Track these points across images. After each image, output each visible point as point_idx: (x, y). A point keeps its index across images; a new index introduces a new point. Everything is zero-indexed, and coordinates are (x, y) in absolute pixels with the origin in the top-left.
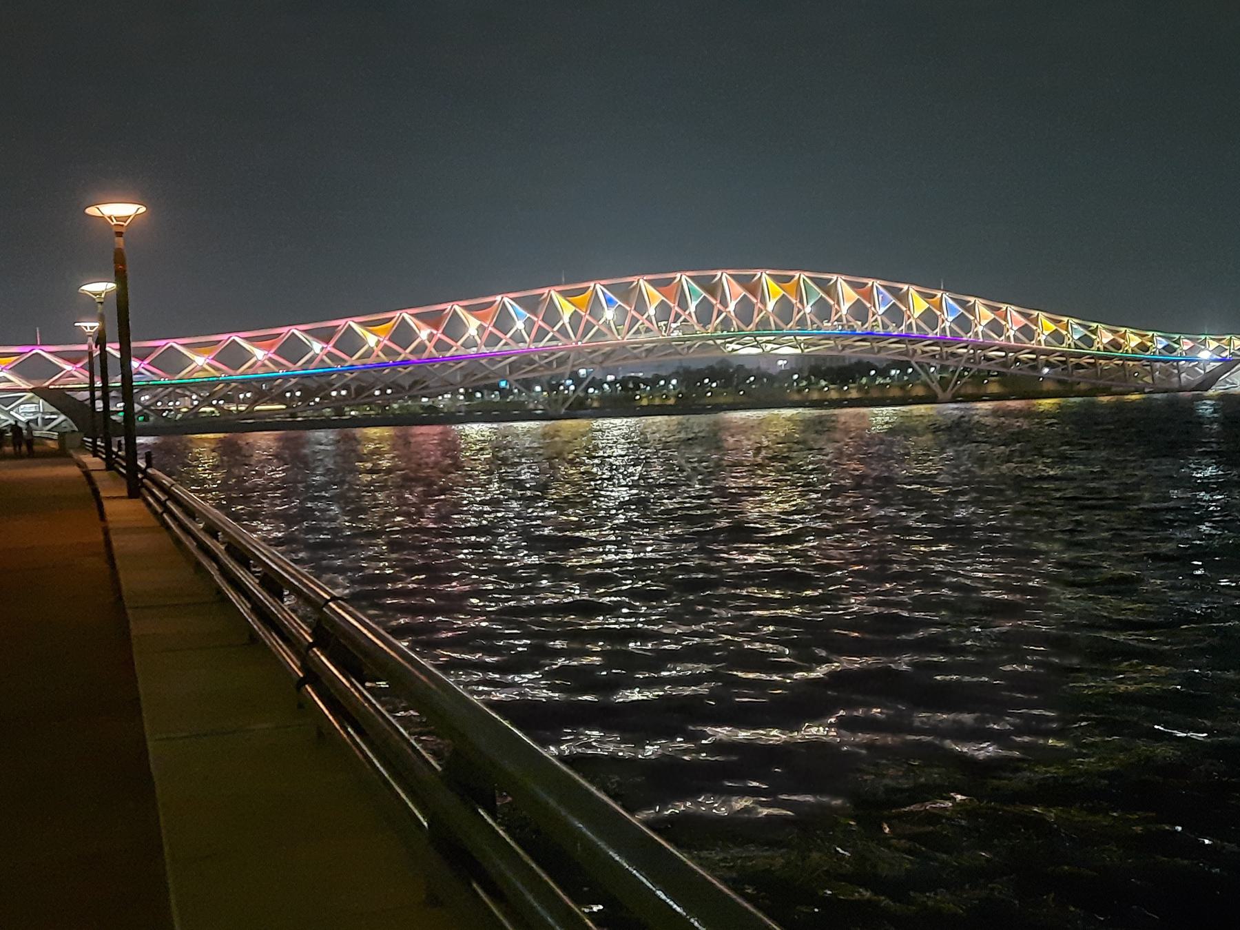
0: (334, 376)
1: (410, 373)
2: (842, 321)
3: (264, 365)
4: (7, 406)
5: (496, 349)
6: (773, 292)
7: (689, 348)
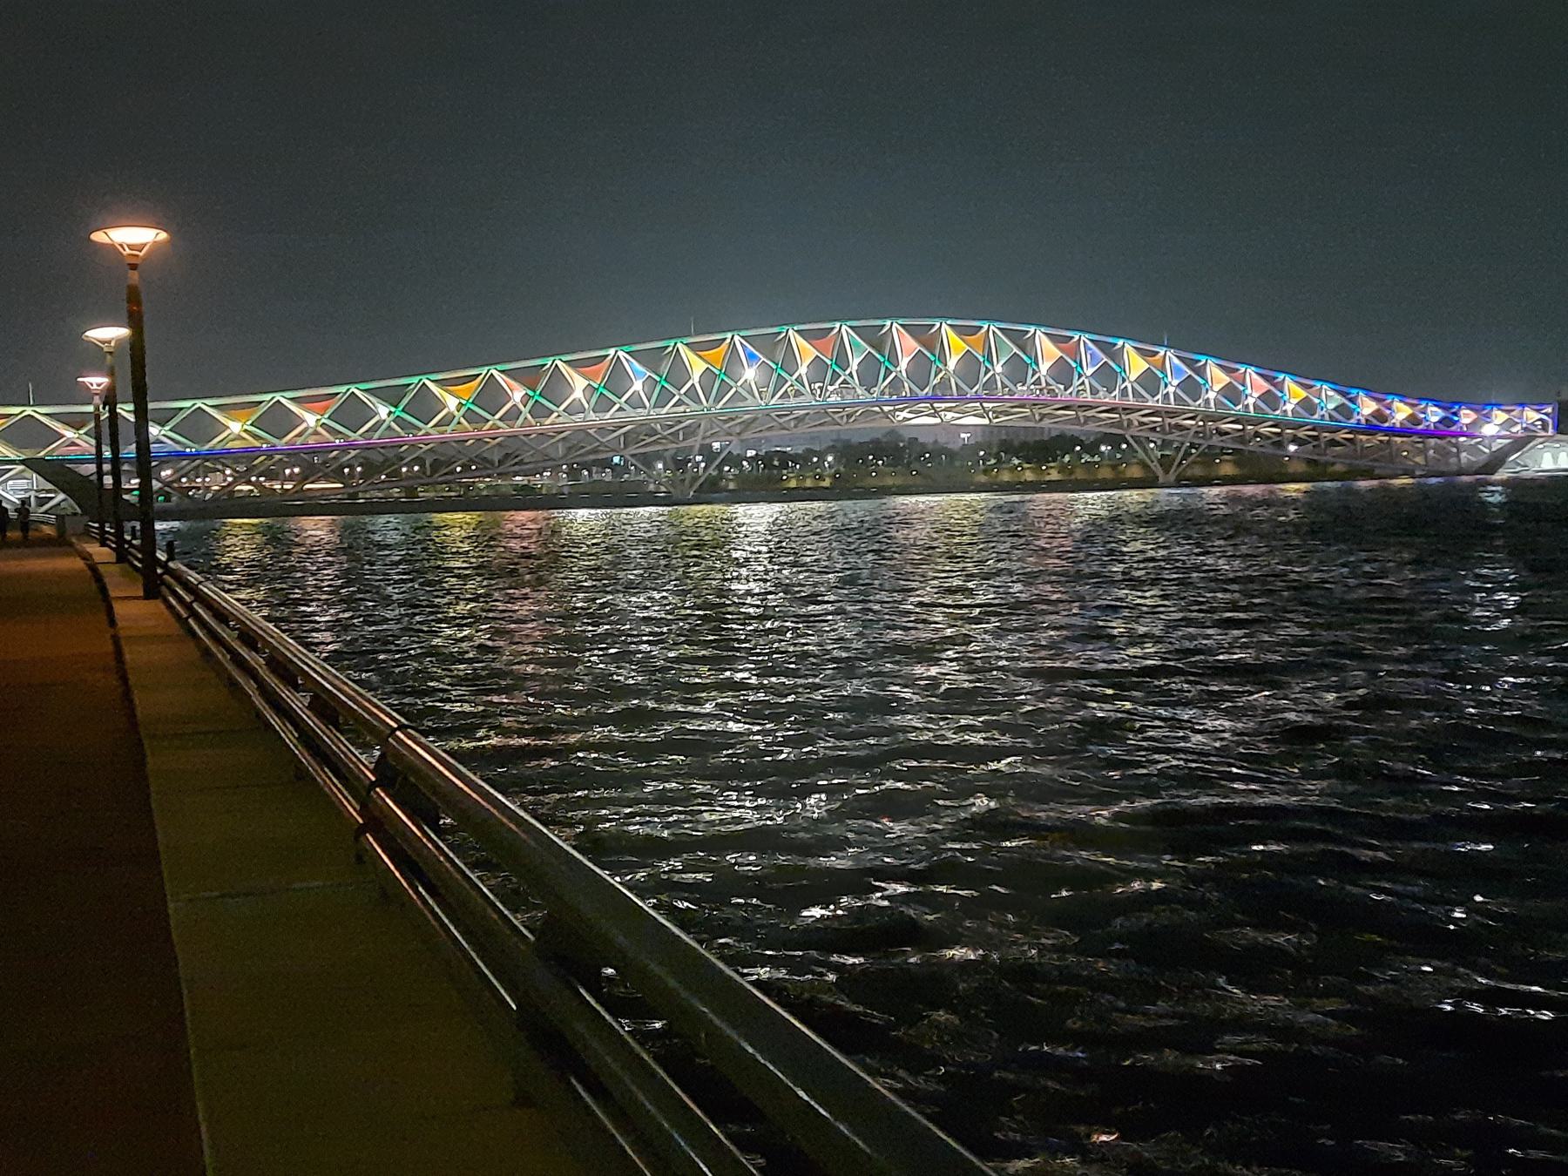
0: (471, 442)
6: (955, 347)
7: (849, 416)
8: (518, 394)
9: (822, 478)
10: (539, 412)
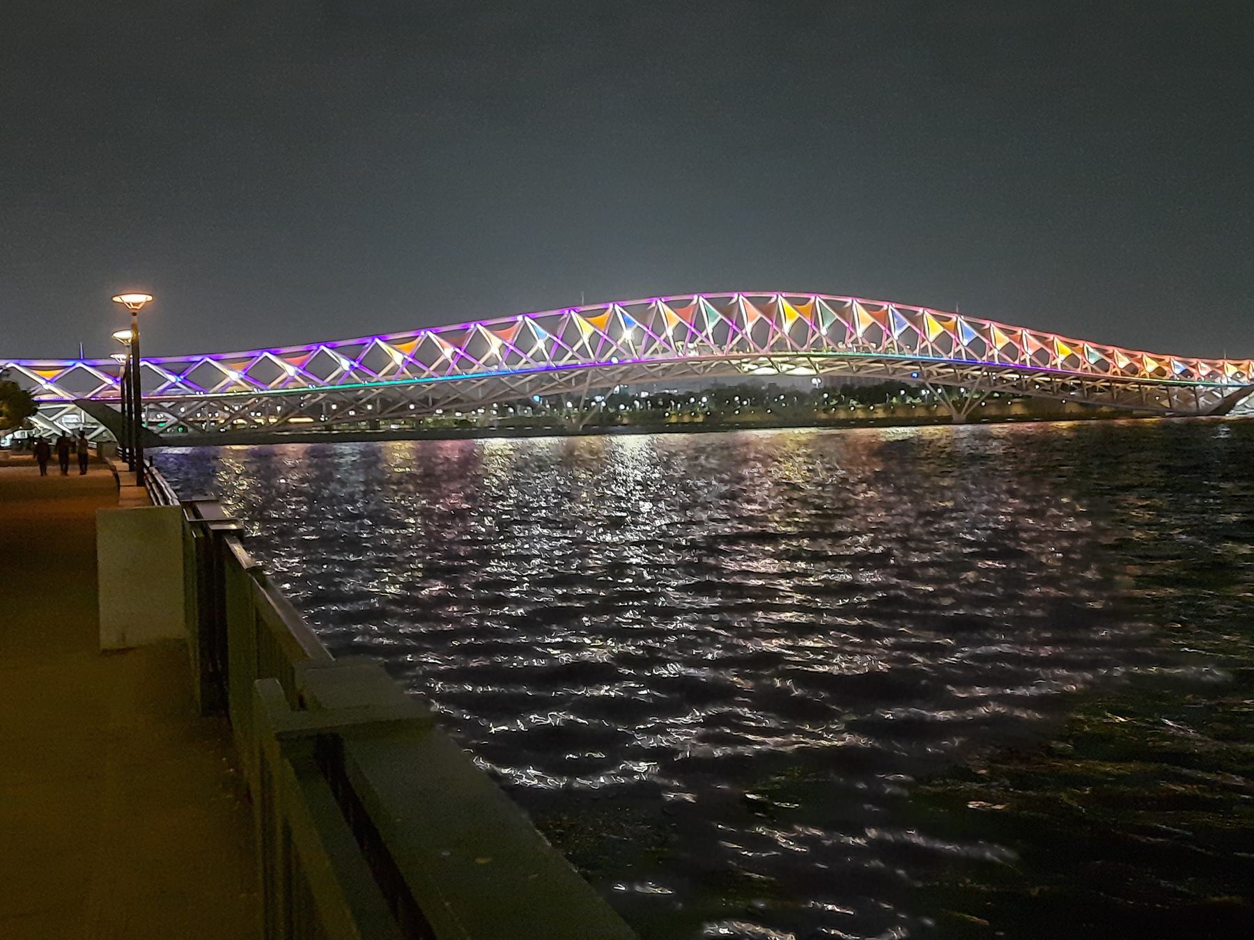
0: (412, 387)
1: (433, 389)
2: (858, 343)
3: (294, 380)
4: (50, 417)
5: (517, 367)
6: (790, 315)
7: (705, 367)
8: (448, 352)
9: (696, 415)
10: (560, 352)
